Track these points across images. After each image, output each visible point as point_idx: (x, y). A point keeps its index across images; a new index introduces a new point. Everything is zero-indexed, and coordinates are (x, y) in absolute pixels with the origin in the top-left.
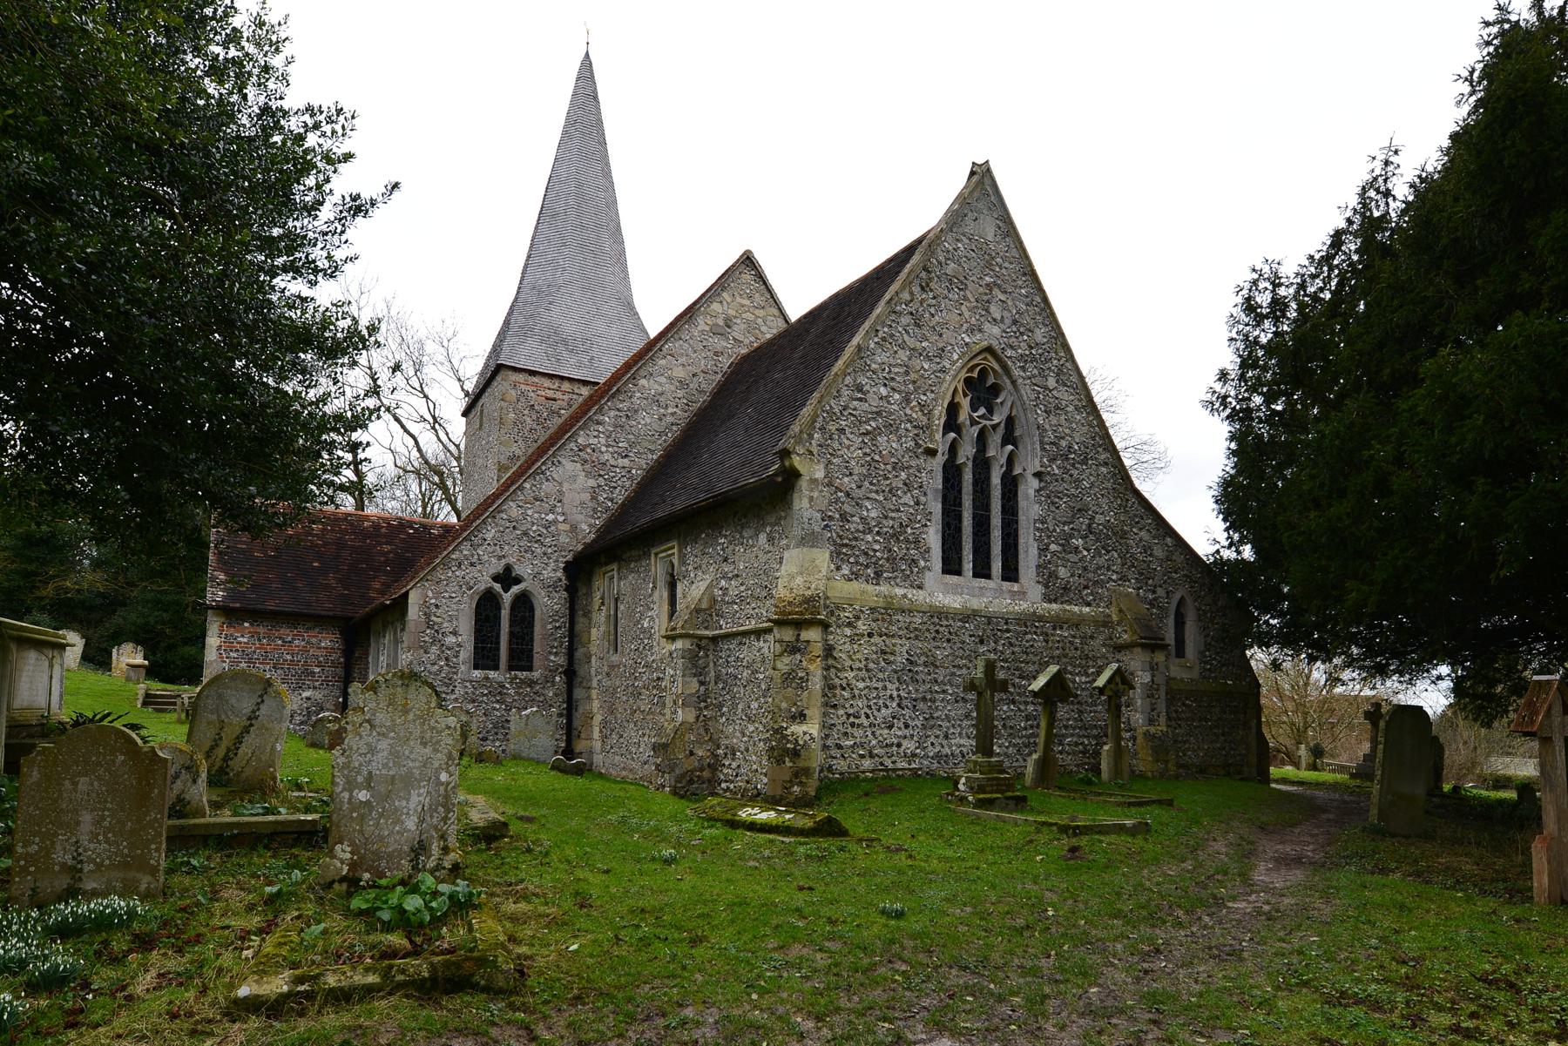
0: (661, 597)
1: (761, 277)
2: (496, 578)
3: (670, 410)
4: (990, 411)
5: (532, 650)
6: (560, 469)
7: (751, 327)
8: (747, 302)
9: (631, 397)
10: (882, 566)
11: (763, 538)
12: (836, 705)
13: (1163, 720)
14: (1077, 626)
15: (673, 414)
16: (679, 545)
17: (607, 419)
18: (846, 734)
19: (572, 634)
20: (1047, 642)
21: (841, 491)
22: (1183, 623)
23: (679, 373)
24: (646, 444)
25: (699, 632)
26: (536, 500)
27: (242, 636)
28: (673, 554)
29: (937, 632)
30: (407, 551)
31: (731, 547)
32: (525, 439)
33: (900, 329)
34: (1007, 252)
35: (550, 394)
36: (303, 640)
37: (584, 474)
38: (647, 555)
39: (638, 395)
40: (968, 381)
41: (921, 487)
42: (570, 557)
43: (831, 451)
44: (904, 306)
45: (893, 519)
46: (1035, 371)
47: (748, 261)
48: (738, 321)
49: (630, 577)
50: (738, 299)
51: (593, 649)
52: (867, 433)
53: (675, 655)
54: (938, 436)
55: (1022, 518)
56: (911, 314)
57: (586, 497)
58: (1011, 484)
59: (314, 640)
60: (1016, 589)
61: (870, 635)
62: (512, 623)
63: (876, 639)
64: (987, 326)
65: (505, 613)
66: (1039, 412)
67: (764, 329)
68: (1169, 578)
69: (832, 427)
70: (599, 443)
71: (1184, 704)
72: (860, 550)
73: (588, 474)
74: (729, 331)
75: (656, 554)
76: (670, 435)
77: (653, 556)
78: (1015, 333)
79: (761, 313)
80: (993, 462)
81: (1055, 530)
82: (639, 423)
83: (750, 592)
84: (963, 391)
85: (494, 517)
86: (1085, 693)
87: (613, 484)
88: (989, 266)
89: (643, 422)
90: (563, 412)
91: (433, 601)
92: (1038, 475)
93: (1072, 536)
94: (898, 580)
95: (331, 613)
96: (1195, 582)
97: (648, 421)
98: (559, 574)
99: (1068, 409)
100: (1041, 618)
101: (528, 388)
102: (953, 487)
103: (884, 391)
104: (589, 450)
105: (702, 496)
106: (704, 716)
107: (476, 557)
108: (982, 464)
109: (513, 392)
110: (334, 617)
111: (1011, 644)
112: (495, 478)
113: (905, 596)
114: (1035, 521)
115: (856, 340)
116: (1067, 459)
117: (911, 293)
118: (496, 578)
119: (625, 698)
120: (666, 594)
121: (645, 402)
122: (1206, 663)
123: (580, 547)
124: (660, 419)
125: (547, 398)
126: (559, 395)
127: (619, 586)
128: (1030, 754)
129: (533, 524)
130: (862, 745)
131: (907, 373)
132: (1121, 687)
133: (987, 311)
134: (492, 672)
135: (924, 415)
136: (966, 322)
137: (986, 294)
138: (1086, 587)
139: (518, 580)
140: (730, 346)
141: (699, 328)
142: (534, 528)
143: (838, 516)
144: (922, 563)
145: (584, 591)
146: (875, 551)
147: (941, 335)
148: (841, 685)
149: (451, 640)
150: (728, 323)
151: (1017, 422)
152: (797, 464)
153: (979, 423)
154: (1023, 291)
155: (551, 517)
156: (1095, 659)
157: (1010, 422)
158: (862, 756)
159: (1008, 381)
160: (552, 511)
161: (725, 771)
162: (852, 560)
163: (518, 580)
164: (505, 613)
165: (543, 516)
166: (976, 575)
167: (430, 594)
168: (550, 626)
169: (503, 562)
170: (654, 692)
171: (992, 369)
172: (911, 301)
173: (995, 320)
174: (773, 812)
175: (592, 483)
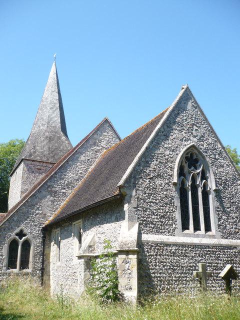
1: (111, 126)
2: (17, 235)
28: (80, 224)
35: (39, 167)
40: (186, 158)
45: (162, 209)
51: (51, 260)
58: (206, 195)
77: (73, 225)
108: (194, 188)
115: (146, 145)
118: (17, 235)
146: (156, 222)
163: (25, 235)
164: (20, 247)
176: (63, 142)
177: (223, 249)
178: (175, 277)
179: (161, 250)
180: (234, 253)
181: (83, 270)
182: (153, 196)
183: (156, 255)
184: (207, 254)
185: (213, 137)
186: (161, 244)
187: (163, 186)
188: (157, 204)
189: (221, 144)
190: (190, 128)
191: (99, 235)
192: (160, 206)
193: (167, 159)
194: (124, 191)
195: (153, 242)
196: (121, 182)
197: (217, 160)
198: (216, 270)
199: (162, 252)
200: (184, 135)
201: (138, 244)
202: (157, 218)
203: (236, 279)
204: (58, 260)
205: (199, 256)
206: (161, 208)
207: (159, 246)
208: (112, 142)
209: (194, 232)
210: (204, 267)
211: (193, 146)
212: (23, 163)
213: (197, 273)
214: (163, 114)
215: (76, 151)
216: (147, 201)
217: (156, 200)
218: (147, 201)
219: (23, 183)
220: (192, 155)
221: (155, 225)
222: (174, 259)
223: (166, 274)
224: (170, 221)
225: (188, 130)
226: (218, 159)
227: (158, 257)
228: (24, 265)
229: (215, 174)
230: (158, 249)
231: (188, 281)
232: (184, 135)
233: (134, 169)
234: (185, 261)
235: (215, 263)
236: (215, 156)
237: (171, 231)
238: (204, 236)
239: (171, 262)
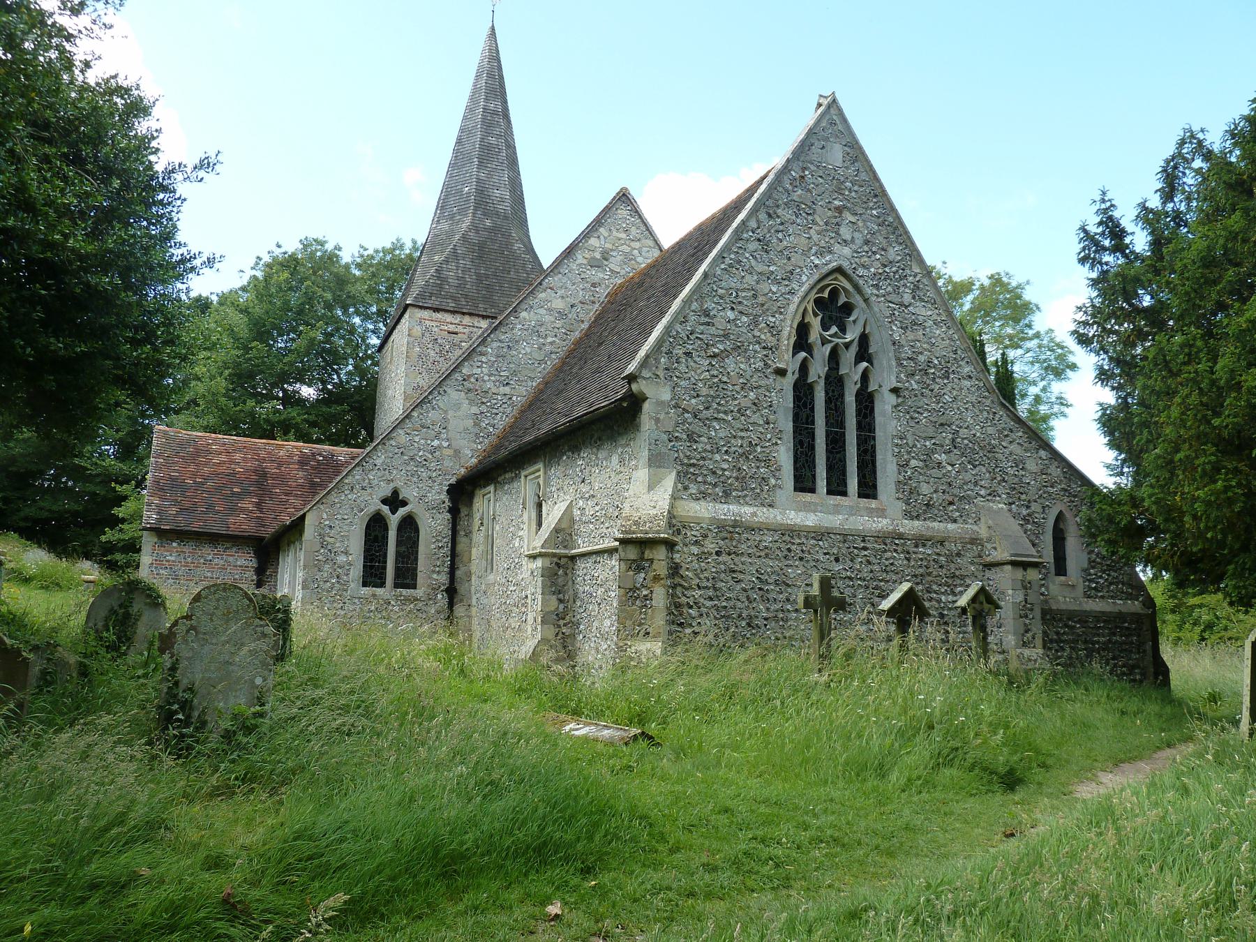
1: (636, 212)
2: (384, 501)
3: (549, 340)
4: (843, 329)
5: (416, 569)
6: (445, 398)
7: (629, 258)
8: (623, 236)
9: (512, 329)
10: (731, 485)
11: (615, 459)
12: (682, 623)
13: (1039, 642)
14: (942, 543)
15: (551, 343)
16: (545, 467)
17: (490, 350)
19: (454, 554)
20: (908, 559)
21: (688, 412)
22: (1064, 539)
23: (558, 304)
24: (527, 372)
25: (558, 551)
26: (423, 427)
28: (539, 477)
29: (789, 550)
31: (588, 469)
32: (429, 371)
33: (747, 255)
34: (856, 175)
35: (452, 328)
36: (222, 559)
37: (467, 402)
38: (517, 476)
40: (818, 302)
41: (770, 406)
42: (453, 480)
45: (742, 438)
46: (889, 289)
47: (624, 197)
48: (614, 254)
51: (473, 568)
52: (714, 356)
54: (788, 356)
55: (879, 434)
56: (759, 240)
57: (469, 423)
58: (866, 401)
59: (231, 559)
60: (873, 506)
61: (718, 553)
62: (399, 543)
63: (724, 558)
64: (836, 247)
66: (894, 328)
67: (640, 259)
68: (1044, 493)
69: (679, 351)
70: (482, 372)
71: (1066, 626)
72: (708, 469)
73: (471, 402)
74: (606, 263)
75: (526, 476)
76: (549, 363)
78: (867, 252)
79: (637, 245)
80: (815, 385)
81: (915, 446)
82: (520, 353)
84: (813, 310)
85: (384, 444)
86: (953, 613)
87: (494, 411)
88: (839, 191)
89: (523, 352)
90: (463, 344)
91: (327, 523)
92: (895, 391)
93: (933, 451)
94: (747, 499)
96: (1075, 496)
97: (528, 350)
98: (444, 496)
99: (926, 324)
100: (901, 536)
101: (434, 324)
102: (805, 405)
103: (731, 315)
104: (472, 380)
105: (563, 420)
106: (563, 633)
107: (367, 481)
108: (835, 382)
109: (418, 328)
110: (249, 538)
111: (869, 563)
113: (754, 514)
114: (894, 437)
115: (704, 267)
116: (926, 374)
117: (758, 221)
118: (384, 501)
120: (534, 515)
121: (525, 332)
123: (463, 471)
124: (540, 349)
126: (460, 329)
127: (495, 506)
131: (755, 296)
132: (986, 606)
133: (837, 233)
134: (379, 590)
135: (773, 335)
136: (815, 245)
137: (836, 217)
138: (951, 503)
139: (404, 503)
140: (607, 277)
142: (420, 454)
143: (685, 437)
144: (773, 481)
145: (466, 513)
146: (724, 470)
147: (789, 259)
148: (688, 604)
149: (342, 559)
150: (606, 255)
151: (871, 339)
153: (830, 342)
154: (874, 212)
155: (436, 443)
156: (962, 577)
157: (864, 340)
159: (858, 297)
160: (437, 437)
162: (700, 479)
163: (404, 503)
165: (429, 442)
166: (830, 492)
167: (325, 516)
168: (433, 546)
169: (392, 485)
171: (844, 289)
173: (845, 241)
175: (475, 410)
176: (518, 258)
181: (539, 591)
186: (734, 527)
189: (921, 261)
197: (906, 307)
201: (671, 525)
214: (763, 178)
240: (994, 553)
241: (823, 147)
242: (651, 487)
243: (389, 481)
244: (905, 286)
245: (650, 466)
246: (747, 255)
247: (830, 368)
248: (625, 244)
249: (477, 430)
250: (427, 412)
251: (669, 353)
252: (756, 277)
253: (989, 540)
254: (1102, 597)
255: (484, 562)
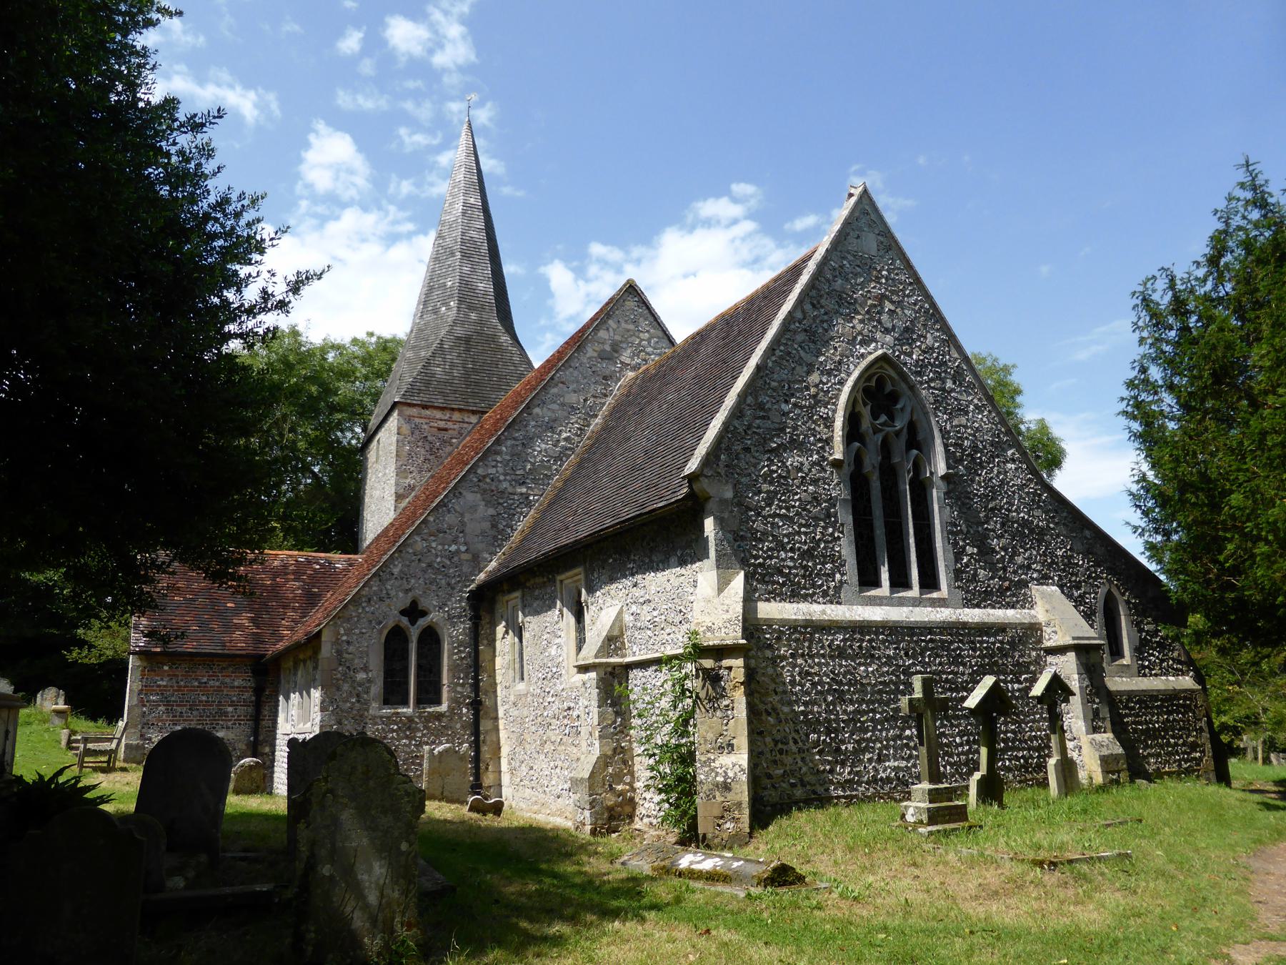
0: (568, 624)
1: (645, 304)
2: (403, 613)
4: (892, 418)
8: (631, 327)
9: (526, 426)
16: (586, 571)
17: (504, 449)
18: (775, 762)
27: (162, 680)
30: (314, 587)
33: (796, 346)
35: (442, 424)
36: (218, 680)
37: (483, 503)
39: (533, 423)
40: (866, 391)
43: (738, 471)
44: (797, 325)
45: (805, 534)
49: (535, 605)
50: (624, 325)
51: (499, 679)
53: (588, 685)
58: (921, 490)
59: (227, 680)
65: (413, 647)
69: (737, 447)
73: (488, 504)
77: (558, 582)
82: (535, 450)
83: (663, 617)
90: (454, 441)
91: (344, 638)
95: (244, 652)
101: (423, 421)
104: (488, 480)
105: (608, 522)
108: (889, 473)
112: (393, 508)
113: (824, 612)
117: (803, 312)
118: (403, 613)
119: (533, 728)
122: (1143, 660)
125: (439, 429)
126: (450, 425)
128: (970, 773)
129: (437, 556)
130: (792, 773)
141: (588, 356)
142: (439, 560)
146: (790, 568)
149: (361, 676)
152: (705, 486)
155: (453, 548)
157: (912, 427)
158: (793, 785)
159: (904, 386)
160: (455, 541)
161: (646, 805)
163: (424, 613)
164: (413, 647)
165: (446, 547)
167: (342, 631)
170: (566, 721)
172: (804, 318)
174: (718, 859)
175: (491, 511)
177: (969, 635)
178: (845, 712)
179: (806, 644)
180: (998, 645)
181: (595, 703)
182: (780, 500)
183: (792, 655)
184: (926, 649)
185: (938, 330)
187: (806, 470)
188: (791, 519)
189: (959, 348)
190: (875, 306)
191: (634, 608)
192: (801, 526)
193: (815, 397)
194: (704, 485)
195: (783, 622)
196: (693, 465)
197: (949, 393)
198: (951, 690)
199: (810, 648)
200: (859, 327)
201: (745, 629)
202: (792, 558)
203: (1006, 714)
204: (518, 676)
205: (907, 654)
206: (803, 529)
207: (801, 633)
208: (649, 350)
209: (892, 592)
210: (927, 685)
211: (884, 358)
212: (395, 414)
213: (911, 701)
215: (552, 378)
216: (764, 513)
217: (788, 509)
218: (764, 513)
219: (401, 472)
220: (881, 382)
221: (787, 575)
222: (841, 666)
223: (820, 706)
224: (829, 566)
225: (868, 312)
226: (953, 390)
227: (800, 661)
228: (430, 693)
229: (945, 434)
230: (797, 640)
231: (881, 722)
232: (859, 327)
233: (726, 426)
234: (870, 669)
235: (952, 672)
236: (944, 383)
237: (831, 592)
238: (916, 603)
239: (833, 672)
240: (1055, 637)
241: (858, 237)
242: (720, 590)
243: (407, 591)
244: (945, 372)
245: (718, 568)
246: (796, 346)
247: (883, 458)
248: (634, 335)
249: (493, 533)
250: (443, 516)
251: (728, 449)
252: (805, 369)
253: (1048, 625)
254: (1156, 675)
255: (511, 672)
